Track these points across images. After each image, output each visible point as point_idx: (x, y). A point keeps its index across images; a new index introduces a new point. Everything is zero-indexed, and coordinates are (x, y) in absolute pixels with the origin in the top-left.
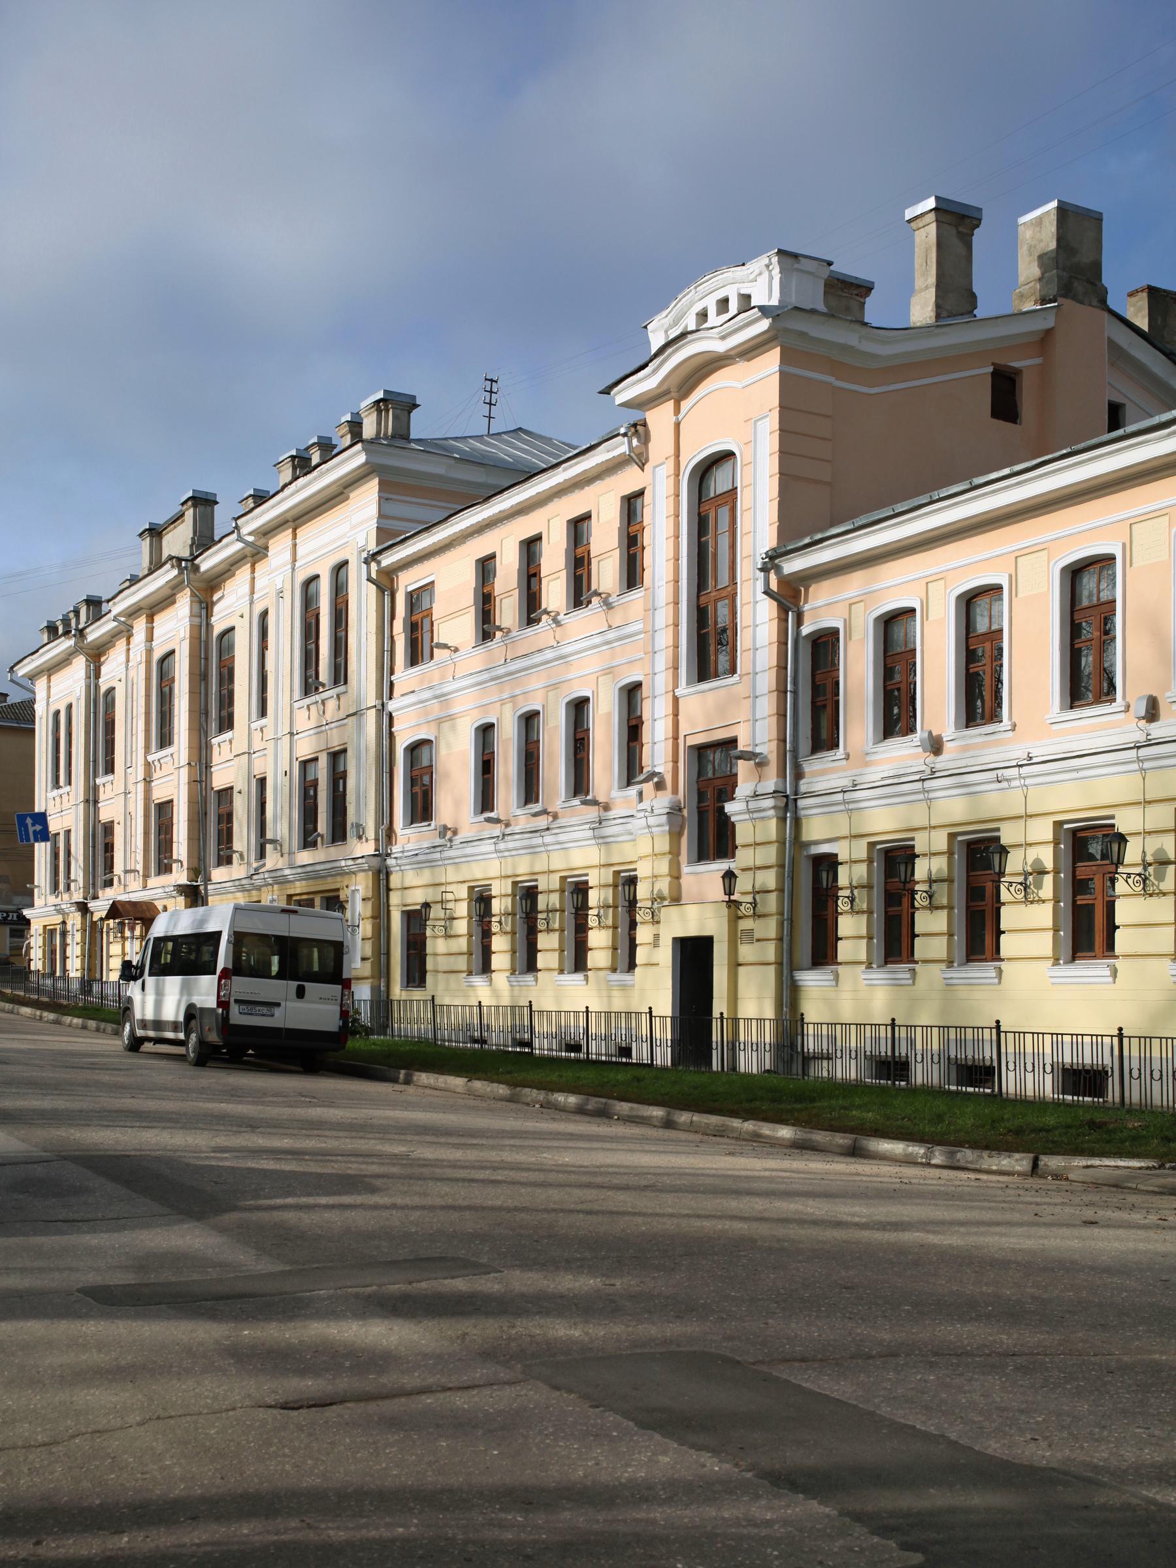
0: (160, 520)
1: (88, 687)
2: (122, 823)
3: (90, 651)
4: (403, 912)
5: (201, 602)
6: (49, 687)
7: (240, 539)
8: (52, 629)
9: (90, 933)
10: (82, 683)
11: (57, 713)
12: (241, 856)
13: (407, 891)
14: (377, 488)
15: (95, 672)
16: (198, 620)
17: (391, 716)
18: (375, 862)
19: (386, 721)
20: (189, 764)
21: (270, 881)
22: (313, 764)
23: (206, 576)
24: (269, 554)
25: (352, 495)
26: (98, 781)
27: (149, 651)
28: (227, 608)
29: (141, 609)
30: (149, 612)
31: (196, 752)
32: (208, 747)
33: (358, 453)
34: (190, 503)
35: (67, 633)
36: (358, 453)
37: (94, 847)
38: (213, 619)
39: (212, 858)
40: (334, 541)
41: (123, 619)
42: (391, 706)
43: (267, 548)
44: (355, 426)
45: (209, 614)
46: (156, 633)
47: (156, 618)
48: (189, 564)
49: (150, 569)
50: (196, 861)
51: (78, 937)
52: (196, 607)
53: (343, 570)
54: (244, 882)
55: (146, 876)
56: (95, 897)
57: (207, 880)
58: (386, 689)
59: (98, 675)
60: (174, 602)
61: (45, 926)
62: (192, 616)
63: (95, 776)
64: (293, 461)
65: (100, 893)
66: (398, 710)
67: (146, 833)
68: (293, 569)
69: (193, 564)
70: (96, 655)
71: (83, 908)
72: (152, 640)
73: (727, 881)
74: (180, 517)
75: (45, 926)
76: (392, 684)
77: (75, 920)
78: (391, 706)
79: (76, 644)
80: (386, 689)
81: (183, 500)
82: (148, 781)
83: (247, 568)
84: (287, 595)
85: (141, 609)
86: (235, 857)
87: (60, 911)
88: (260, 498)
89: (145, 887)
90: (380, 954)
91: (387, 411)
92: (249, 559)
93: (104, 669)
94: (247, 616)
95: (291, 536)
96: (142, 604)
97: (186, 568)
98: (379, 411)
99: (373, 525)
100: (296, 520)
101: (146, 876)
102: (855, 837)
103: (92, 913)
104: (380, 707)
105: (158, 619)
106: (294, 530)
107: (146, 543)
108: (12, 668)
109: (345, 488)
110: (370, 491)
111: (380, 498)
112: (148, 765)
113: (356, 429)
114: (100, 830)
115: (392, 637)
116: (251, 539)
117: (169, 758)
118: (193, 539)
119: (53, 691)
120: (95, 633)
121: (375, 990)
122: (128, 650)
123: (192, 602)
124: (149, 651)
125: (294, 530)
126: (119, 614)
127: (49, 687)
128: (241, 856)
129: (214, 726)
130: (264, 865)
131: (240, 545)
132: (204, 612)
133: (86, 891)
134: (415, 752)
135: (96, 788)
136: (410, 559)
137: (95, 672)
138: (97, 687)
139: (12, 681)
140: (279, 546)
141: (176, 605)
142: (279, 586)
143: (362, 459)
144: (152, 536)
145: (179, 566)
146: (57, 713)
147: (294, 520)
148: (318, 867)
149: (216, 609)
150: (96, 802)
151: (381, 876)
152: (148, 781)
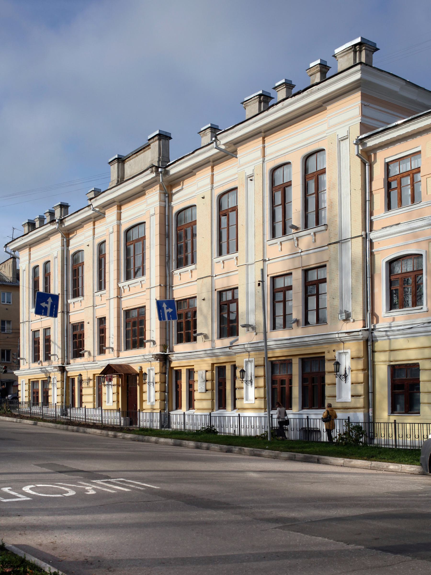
0: (124, 154)
1: (63, 251)
2: (91, 323)
3: (64, 232)
4: (389, 366)
5: (165, 194)
6: (30, 254)
7: (217, 148)
8: (32, 225)
9: (66, 383)
10: (60, 249)
11: (36, 268)
12: (89, 353)
13: (393, 352)
14: (360, 98)
15: (66, 243)
16: (164, 203)
17: (371, 241)
18: (366, 334)
19: (368, 245)
20: (160, 285)
21: (249, 349)
22: (48, 330)
23: (173, 177)
24: (106, 216)
25: (328, 108)
26: (69, 301)
27: (119, 226)
28: (189, 194)
29: (114, 202)
30: (118, 204)
31: (163, 278)
32: (171, 276)
33: (356, 72)
34: (157, 138)
35: (52, 221)
36: (356, 72)
37: (67, 336)
38: (173, 203)
39: (174, 338)
40: (284, 148)
41: (97, 209)
42: (372, 236)
43: (105, 214)
44: (52, 214)
45: (170, 201)
46: (123, 216)
47: (123, 207)
48: (163, 169)
49: (118, 181)
50: (164, 340)
51: (59, 385)
52: (163, 196)
53: (48, 264)
54: (246, 346)
55: (119, 350)
56: (68, 364)
57: (172, 351)
58: (368, 224)
59: (68, 245)
60: (145, 194)
61: (29, 380)
62: (160, 201)
63: (67, 299)
64: (260, 98)
65: (71, 361)
66: (375, 239)
67: (119, 327)
68: (263, 161)
69: (165, 170)
70: (67, 234)
71: (62, 369)
72: (120, 220)
73: (242, 373)
74: (146, 147)
75: (29, 380)
76: (371, 222)
77: (56, 376)
78: (372, 236)
79: (58, 227)
80: (368, 224)
81: (150, 137)
82: (119, 298)
83: (91, 224)
84: (258, 179)
85: (114, 202)
86: (86, 354)
87: (46, 372)
88: (98, 193)
89: (118, 356)
90: (369, 392)
91: (360, 51)
92: (211, 163)
93: (71, 242)
94: (91, 245)
95: (261, 142)
96: (116, 200)
97: (161, 172)
98: (355, 52)
99: (359, 119)
100: (265, 132)
101: (119, 350)
102: (391, 351)
103: (67, 372)
104: (364, 236)
105: (124, 208)
106: (264, 138)
107: (114, 168)
108: (6, 245)
109: (49, 235)
110: (356, 99)
111: (362, 104)
112: (119, 288)
113: (324, 70)
114: (70, 327)
115: (371, 192)
116: (223, 147)
117: (139, 283)
118: (159, 158)
119: (32, 256)
120: (68, 222)
121: (367, 416)
122: (94, 229)
123: (160, 193)
124: (119, 226)
125: (264, 138)
126: (96, 207)
127: (30, 254)
128: (89, 353)
129: (174, 264)
130: (238, 340)
131: (91, 212)
132: (167, 199)
133: (63, 358)
134: (392, 265)
135: (68, 305)
136: (389, 142)
137: (66, 243)
138: (68, 251)
139: (6, 252)
140: (111, 214)
141: (146, 197)
142: (55, 255)
143: (358, 76)
144: (119, 162)
145: (157, 171)
146: (36, 268)
147: (265, 132)
148: (306, 339)
149: (174, 197)
150: (68, 312)
151: (369, 342)
152: (119, 298)
